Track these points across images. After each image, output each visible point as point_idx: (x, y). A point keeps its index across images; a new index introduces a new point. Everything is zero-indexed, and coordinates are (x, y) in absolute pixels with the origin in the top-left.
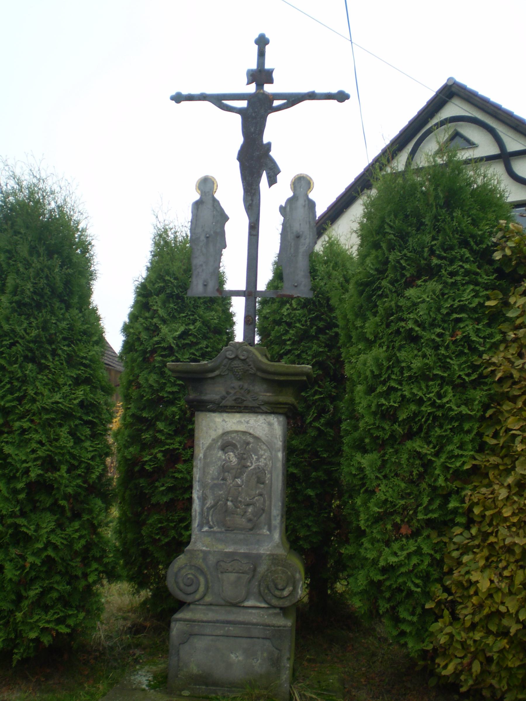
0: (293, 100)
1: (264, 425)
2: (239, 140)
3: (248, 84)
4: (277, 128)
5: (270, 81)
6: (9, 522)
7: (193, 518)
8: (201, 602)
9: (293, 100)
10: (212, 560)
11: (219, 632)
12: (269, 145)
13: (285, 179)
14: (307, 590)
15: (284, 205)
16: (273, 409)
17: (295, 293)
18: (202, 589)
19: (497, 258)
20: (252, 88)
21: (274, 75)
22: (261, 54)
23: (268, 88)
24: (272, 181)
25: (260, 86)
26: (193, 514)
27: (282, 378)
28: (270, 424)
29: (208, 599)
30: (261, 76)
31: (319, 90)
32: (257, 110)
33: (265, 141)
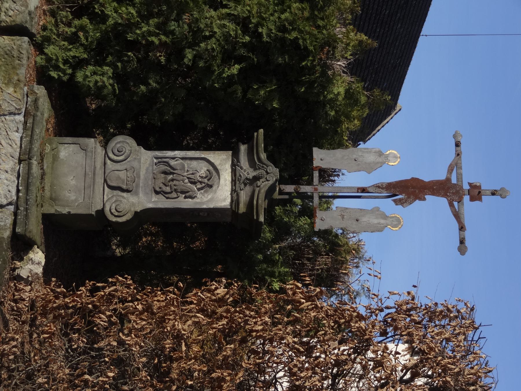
0: (457, 216)
1: (224, 196)
2: (426, 178)
3: (469, 183)
4: (436, 205)
5: (472, 199)
7: (162, 152)
8: (107, 159)
10: (135, 164)
11: (87, 170)
12: (424, 199)
16: (235, 201)
17: (317, 220)
18: (115, 158)
19: (262, 130)
20: (466, 187)
21: (477, 202)
23: (466, 198)
26: (165, 152)
27: (255, 202)
28: (225, 200)
29: (108, 162)
30: (476, 193)
31: (468, 234)
32: (443, 188)
33: (426, 197)
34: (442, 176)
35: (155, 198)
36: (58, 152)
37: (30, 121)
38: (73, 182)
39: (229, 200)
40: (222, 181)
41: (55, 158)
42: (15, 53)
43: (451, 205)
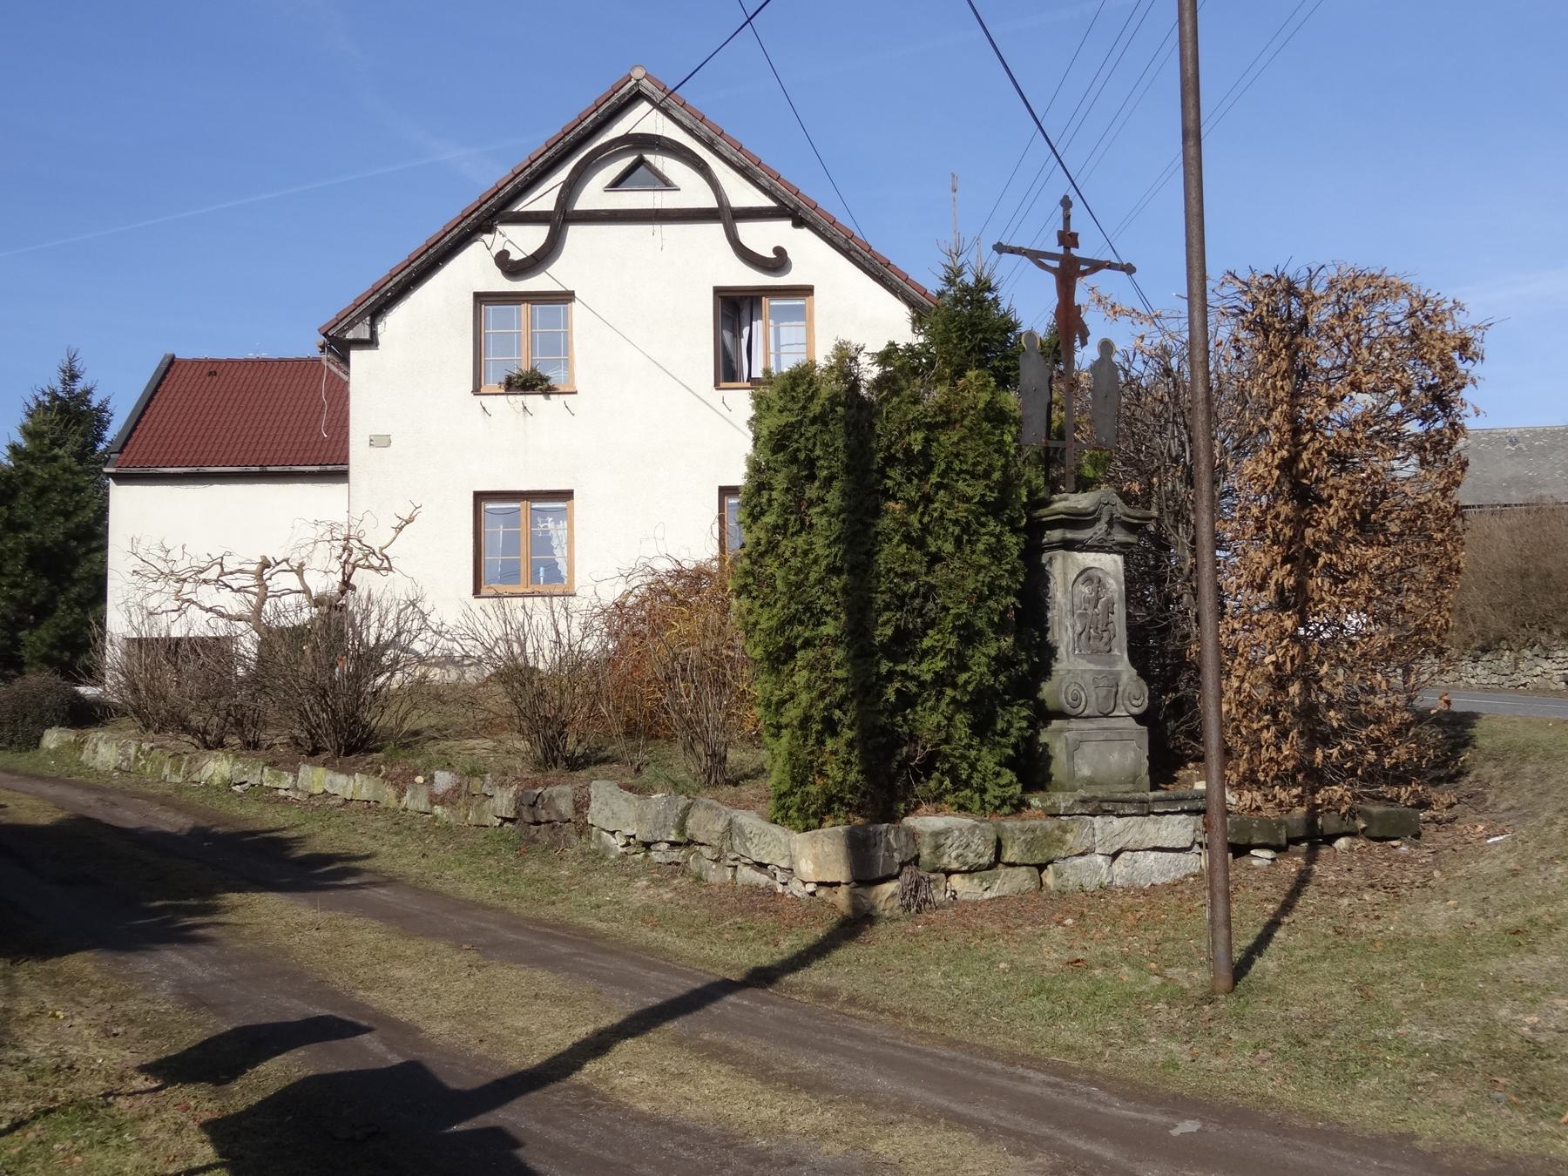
0: (1096, 266)
5: (1076, 245)
6: (706, 1037)
9: (1096, 266)
13: (1094, 341)
14: (1180, 774)
15: (520, 1152)
22: (1067, 219)
24: (1084, 343)
25: (1067, 248)
30: (1068, 238)
34: (1051, 280)
35: (1116, 652)
36: (1084, 778)
37: (1106, 806)
38: (1116, 755)
39: (1115, 556)
40: (1096, 565)
41: (1091, 782)
42: (1030, 836)
43: (1084, 273)
